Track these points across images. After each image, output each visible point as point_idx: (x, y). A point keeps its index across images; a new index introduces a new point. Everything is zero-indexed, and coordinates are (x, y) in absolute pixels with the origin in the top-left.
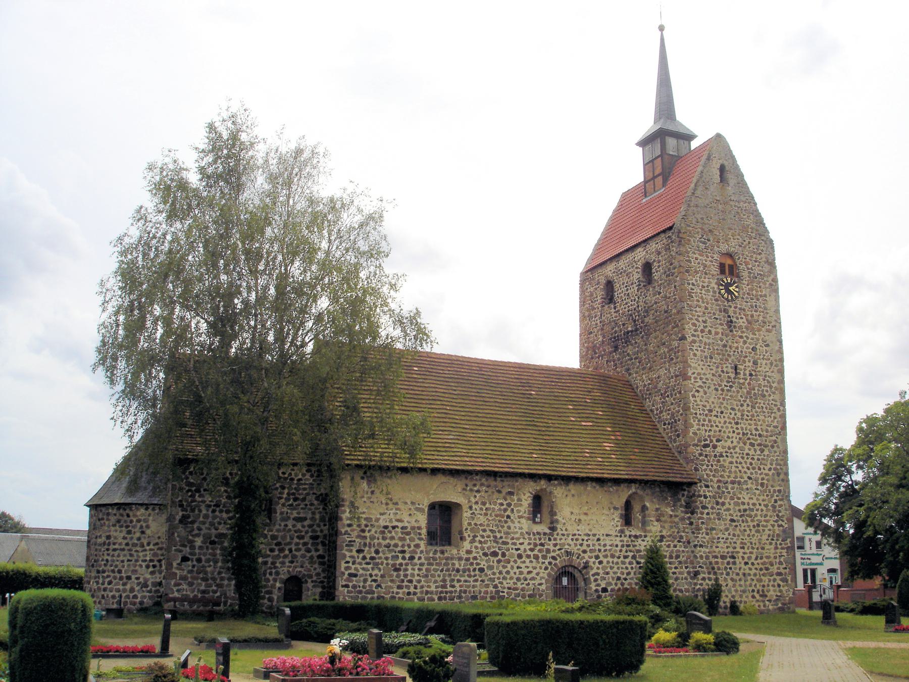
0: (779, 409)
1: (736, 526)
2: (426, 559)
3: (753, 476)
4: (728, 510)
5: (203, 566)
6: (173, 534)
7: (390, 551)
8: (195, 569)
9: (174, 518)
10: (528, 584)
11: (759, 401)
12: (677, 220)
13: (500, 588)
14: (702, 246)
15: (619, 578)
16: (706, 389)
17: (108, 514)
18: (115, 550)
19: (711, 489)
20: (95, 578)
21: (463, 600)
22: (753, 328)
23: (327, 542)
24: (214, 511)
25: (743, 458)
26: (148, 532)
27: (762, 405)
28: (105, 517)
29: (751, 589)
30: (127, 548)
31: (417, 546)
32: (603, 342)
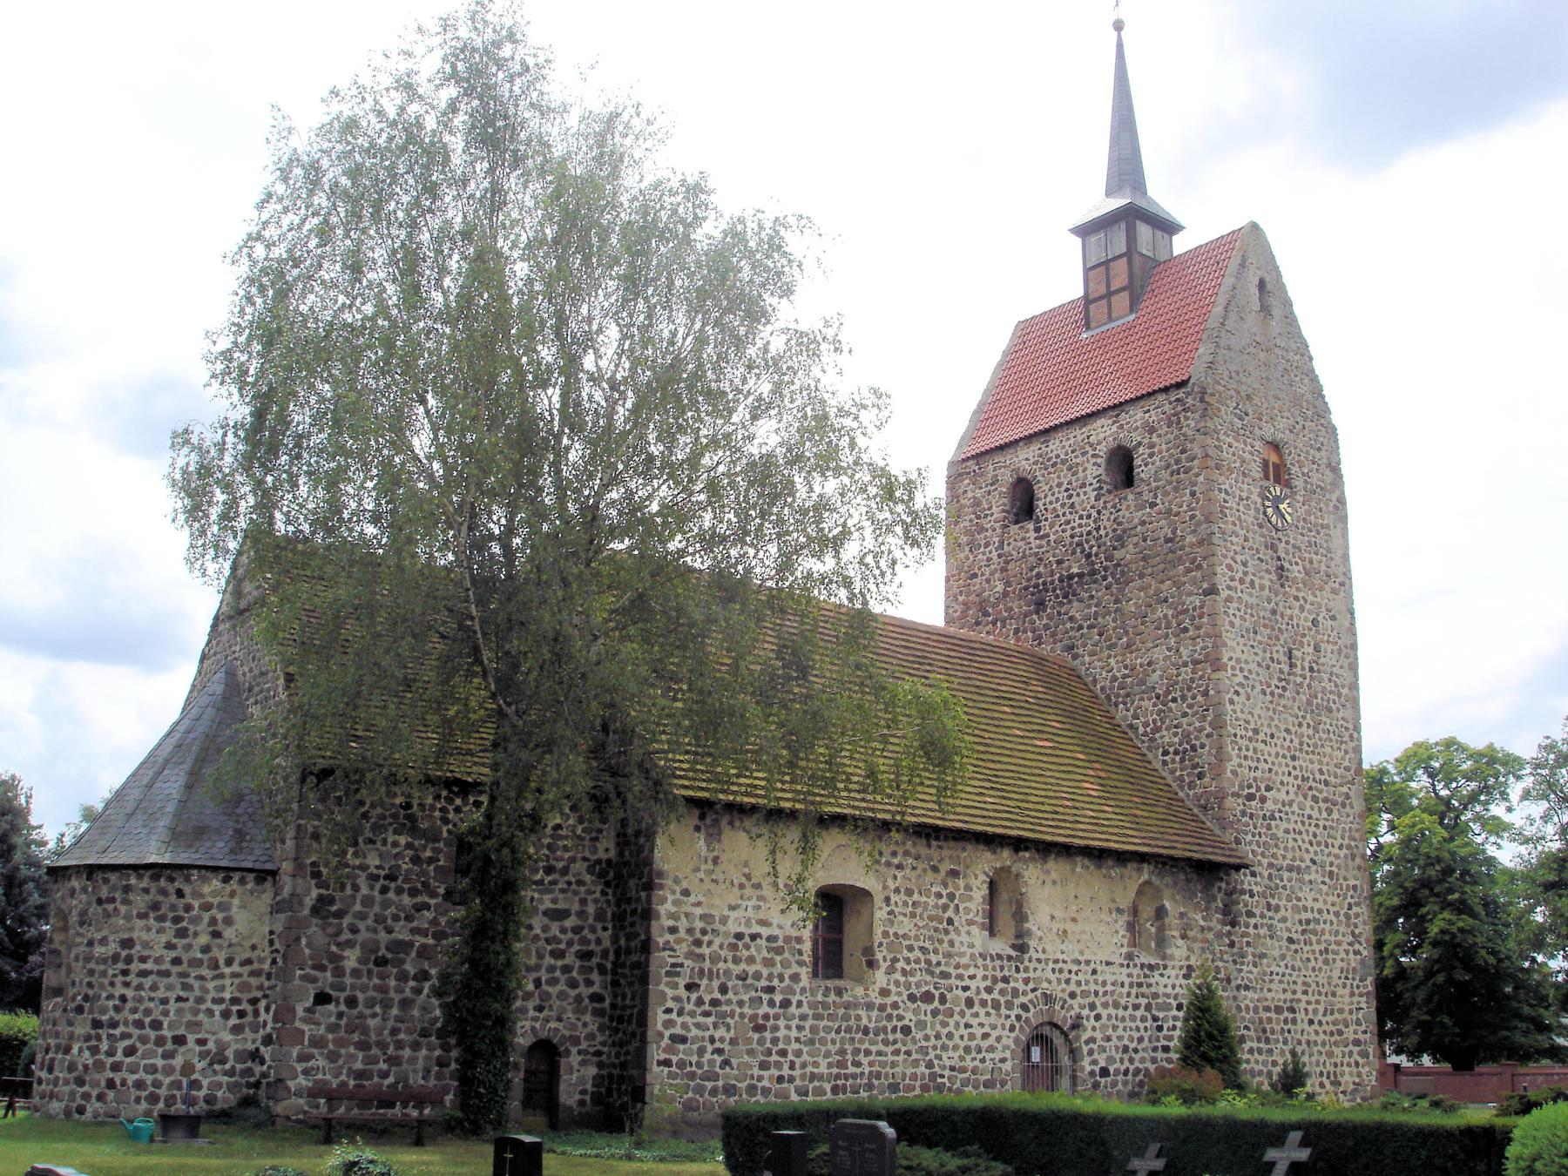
0: (1351, 736)
1: (1296, 951)
2: (812, 1005)
3: (1318, 858)
4: (1284, 920)
5: (361, 1016)
6: (298, 939)
7: (747, 987)
8: (343, 1022)
9: (301, 903)
10: (983, 1060)
11: (1324, 719)
12: (1197, 371)
13: (937, 1069)
14: (1239, 424)
15: (1126, 1049)
16: (1249, 690)
17: (127, 889)
18: (144, 974)
19: (1258, 879)
20: (88, 1038)
21: (875, 1092)
22: (1314, 585)
23: (609, 966)
24: (384, 890)
25: (1303, 823)
26: (229, 933)
27: (1328, 726)
28: (118, 895)
29: (1318, 1070)
30: (175, 969)
31: (795, 978)
32: (1005, 594)
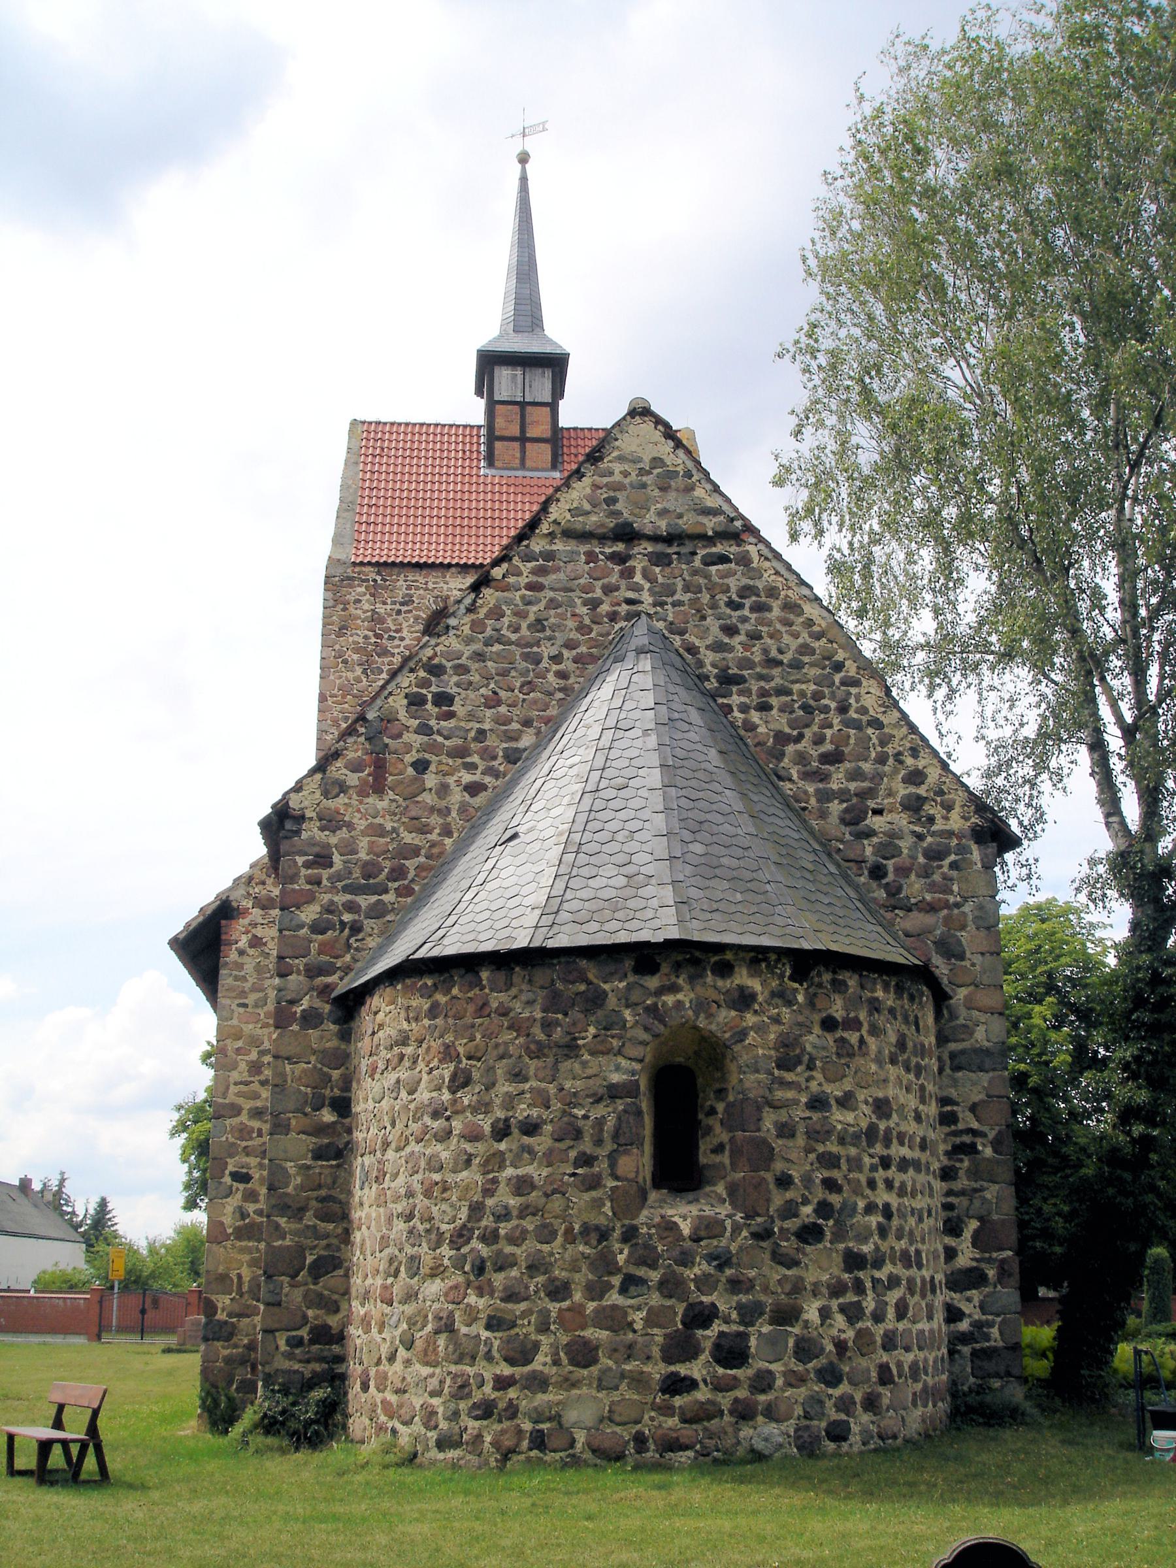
20: (837, 1290)
